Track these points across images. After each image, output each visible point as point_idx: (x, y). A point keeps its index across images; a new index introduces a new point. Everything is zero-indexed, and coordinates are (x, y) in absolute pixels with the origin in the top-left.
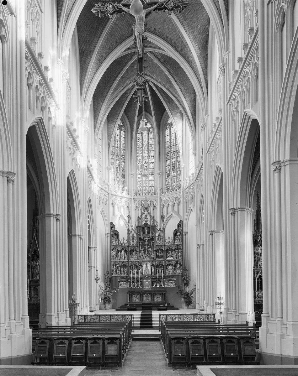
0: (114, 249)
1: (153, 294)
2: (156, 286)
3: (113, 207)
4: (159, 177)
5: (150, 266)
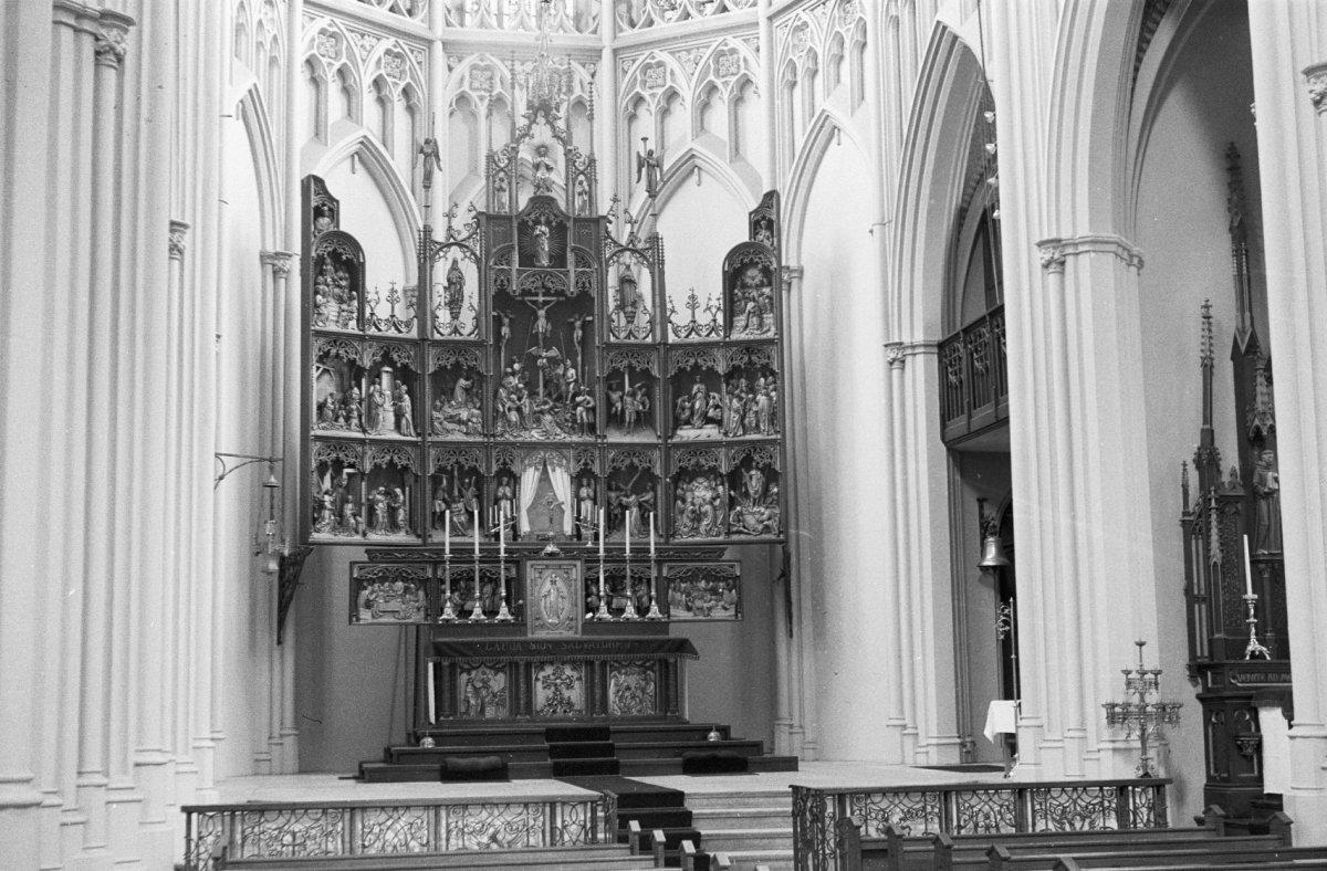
0: (327, 354)
1: (592, 654)
2: (464, 613)
5: (567, 478)
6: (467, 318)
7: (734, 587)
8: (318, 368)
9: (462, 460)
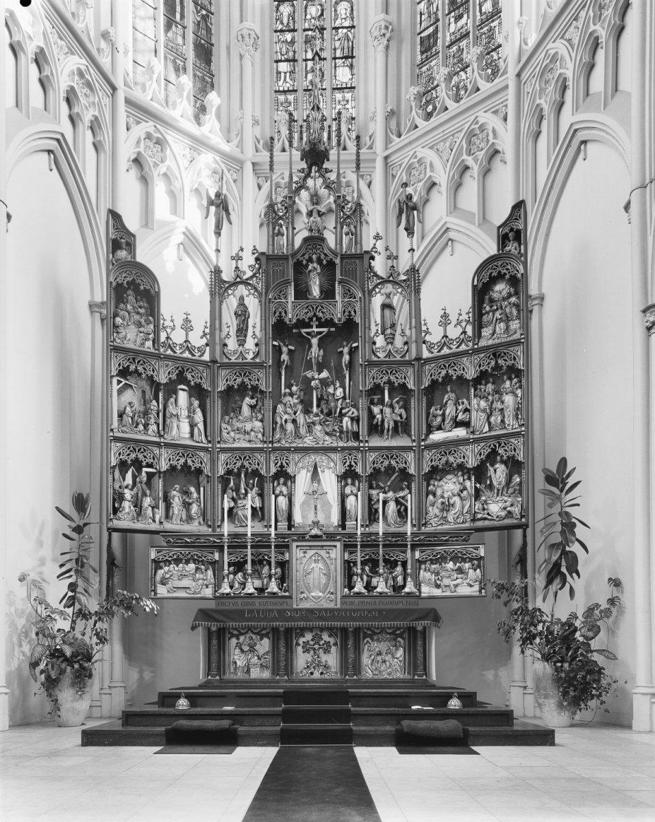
1: (349, 630)
2: (369, 587)
3: (145, 180)
4: (381, 48)
5: (334, 479)
6: (250, 344)
7: (479, 566)
8: (119, 382)
9: (246, 464)
